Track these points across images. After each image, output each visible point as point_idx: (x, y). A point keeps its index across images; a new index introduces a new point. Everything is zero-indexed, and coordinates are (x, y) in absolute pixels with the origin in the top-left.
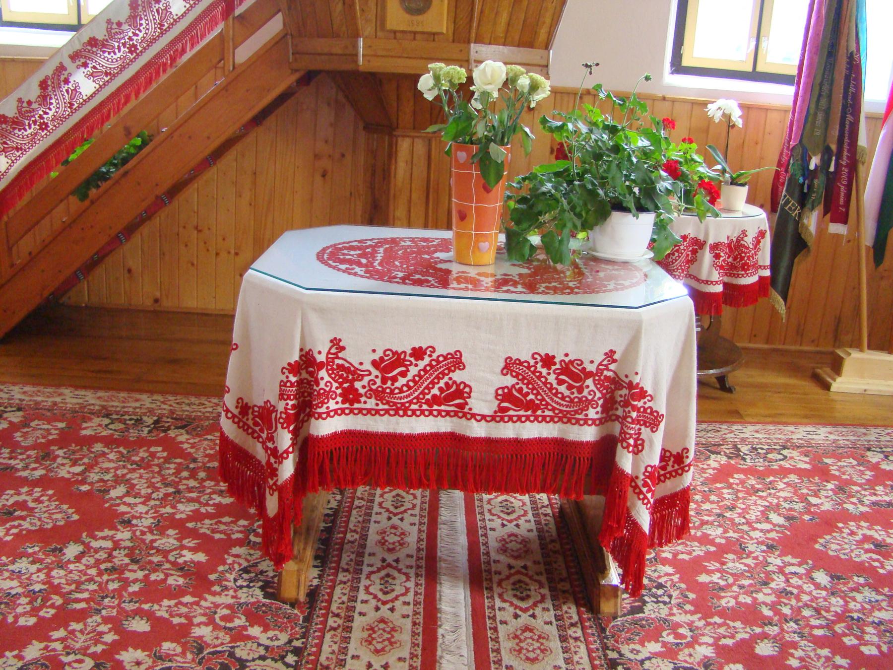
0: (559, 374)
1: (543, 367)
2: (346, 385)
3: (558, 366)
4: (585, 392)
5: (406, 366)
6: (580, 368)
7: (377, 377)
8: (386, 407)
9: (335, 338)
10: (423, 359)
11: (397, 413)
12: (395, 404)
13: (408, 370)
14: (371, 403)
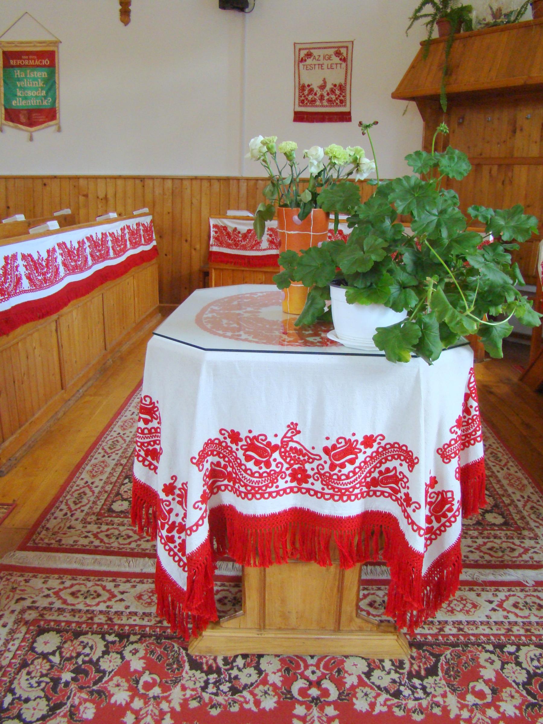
0: (246, 450)
2: (296, 466)
3: (244, 443)
8: (331, 491)
9: (292, 423)
11: (341, 498)
12: (340, 490)
14: (318, 486)
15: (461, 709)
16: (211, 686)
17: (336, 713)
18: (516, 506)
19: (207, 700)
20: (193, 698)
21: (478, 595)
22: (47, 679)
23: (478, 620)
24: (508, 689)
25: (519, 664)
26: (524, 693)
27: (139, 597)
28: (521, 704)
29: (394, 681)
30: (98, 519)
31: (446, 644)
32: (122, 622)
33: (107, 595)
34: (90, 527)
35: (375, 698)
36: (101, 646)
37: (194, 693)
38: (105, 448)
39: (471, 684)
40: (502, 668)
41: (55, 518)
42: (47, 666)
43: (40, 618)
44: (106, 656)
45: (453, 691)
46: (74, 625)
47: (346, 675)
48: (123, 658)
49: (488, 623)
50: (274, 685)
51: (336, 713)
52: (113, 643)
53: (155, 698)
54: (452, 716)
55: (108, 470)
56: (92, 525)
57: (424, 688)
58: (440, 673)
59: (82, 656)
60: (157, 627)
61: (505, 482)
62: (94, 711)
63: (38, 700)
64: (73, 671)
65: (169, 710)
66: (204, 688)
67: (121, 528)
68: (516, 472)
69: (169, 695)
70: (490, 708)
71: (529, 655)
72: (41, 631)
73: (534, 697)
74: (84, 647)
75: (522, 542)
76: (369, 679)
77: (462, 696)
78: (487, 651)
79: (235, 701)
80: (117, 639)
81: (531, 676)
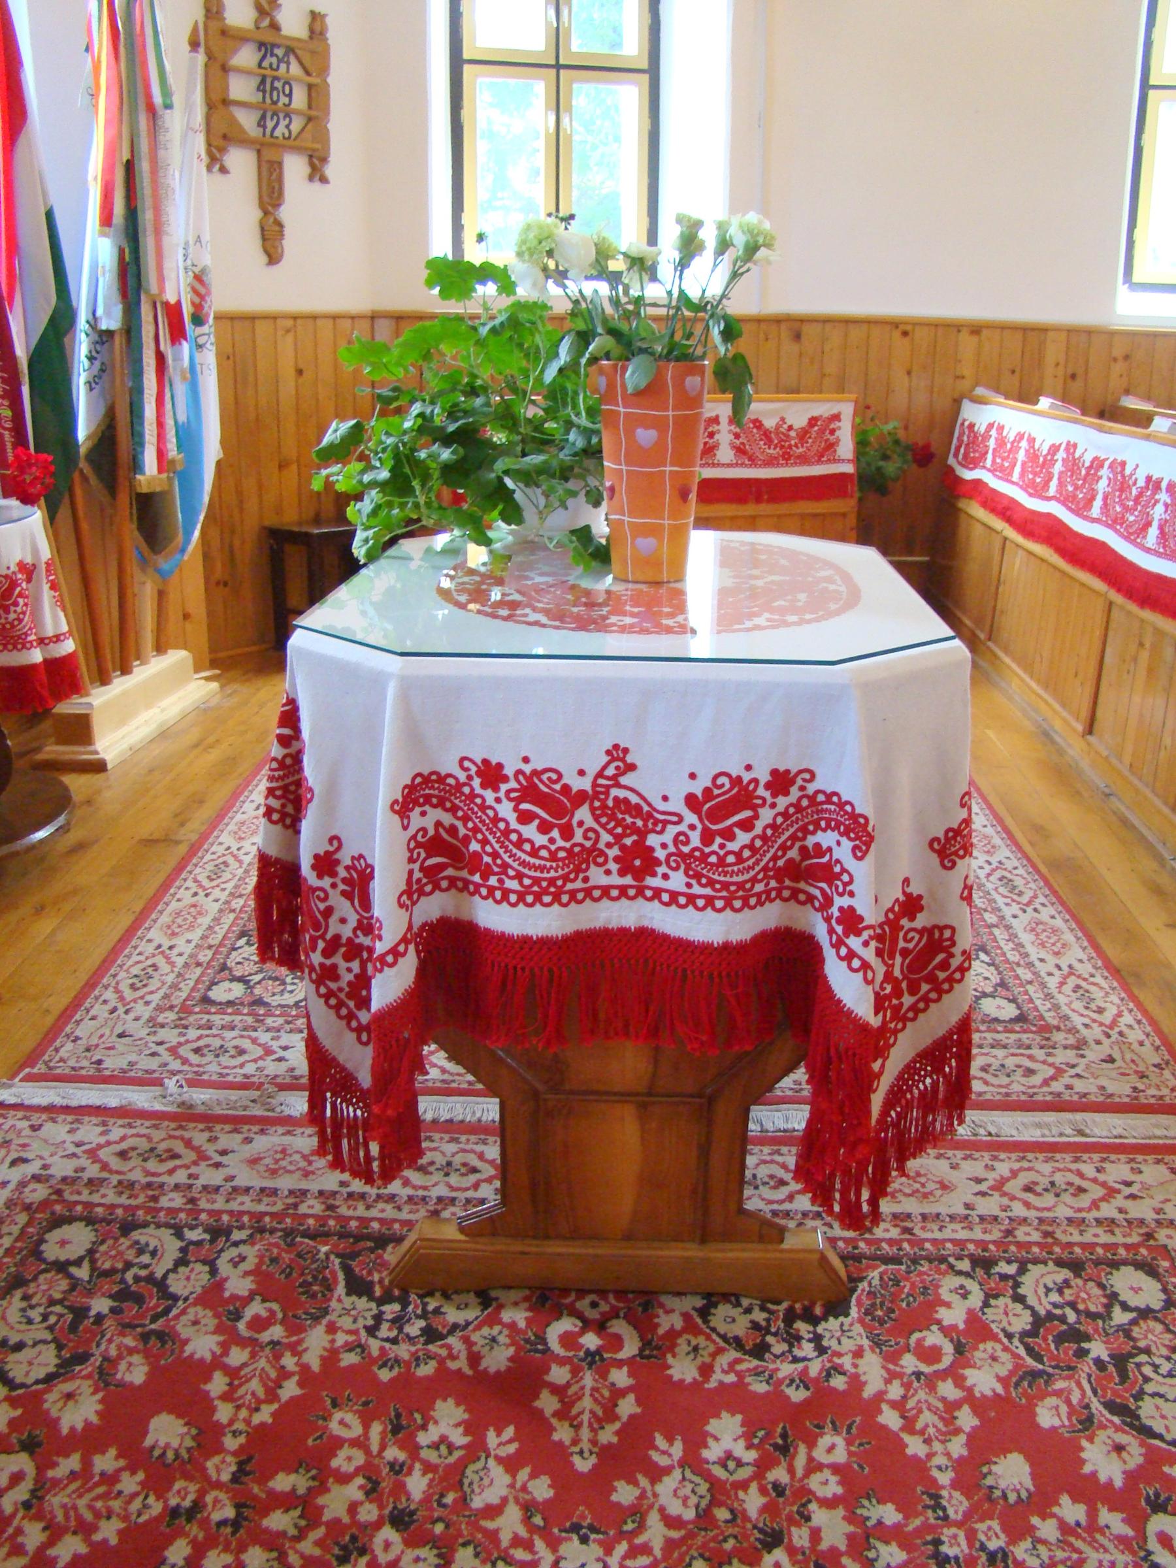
1: (484, 786)
3: (513, 784)
4: (578, 836)
5: (754, 808)
6: (558, 787)
7: (692, 827)
8: (708, 891)
9: (616, 747)
10: (787, 794)
13: (756, 816)
14: (677, 881)
15: (888, 1381)
16: (385, 1326)
17: (630, 1381)
18: (1043, 985)
19: (375, 1353)
20: (349, 1347)
21: (954, 1167)
22: (58, 1309)
23: (943, 1210)
24: (989, 1345)
25: (1020, 1299)
26: (1022, 1351)
27: (254, 1161)
28: (1012, 1373)
29: (755, 1326)
30: (180, 1019)
31: (874, 1257)
32: (216, 1206)
33: (193, 1156)
34: (163, 1034)
35: (714, 1355)
36: (171, 1247)
37: (351, 1338)
38: (199, 878)
39: (916, 1336)
40: (986, 1304)
41: (93, 1018)
42: (64, 1284)
43: (54, 1197)
44: (181, 1269)
45: (877, 1344)
46: (119, 1211)
47: (661, 1312)
48: (214, 1271)
49: (966, 1217)
50: (512, 1326)
51: (630, 1381)
52: (199, 1243)
53: (274, 1343)
54: (868, 1392)
55: (205, 921)
56: (166, 1030)
57: (817, 1339)
58: (854, 1312)
59: (135, 1270)
60: (288, 1215)
61: (1026, 938)
62: (146, 1369)
63: (40, 1347)
64: (111, 1297)
65: (297, 1369)
66: (372, 1331)
67: (229, 1035)
68: (1053, 917)
69: (299, 1342)
70: (944, 1380)
71: (1042, 1282)
72: (57, 1222)
73: (1038, 1358)
74: (141, 1252)
75: (1049, 1054)
76: (706, 1321)
77: (892, 1357)
78: (960, 1273)
79: (430, 1356)
80: (207, 1237)
81: (1038, 1322)
